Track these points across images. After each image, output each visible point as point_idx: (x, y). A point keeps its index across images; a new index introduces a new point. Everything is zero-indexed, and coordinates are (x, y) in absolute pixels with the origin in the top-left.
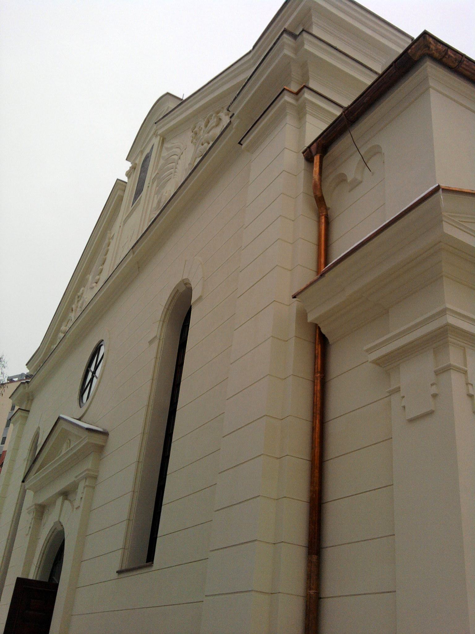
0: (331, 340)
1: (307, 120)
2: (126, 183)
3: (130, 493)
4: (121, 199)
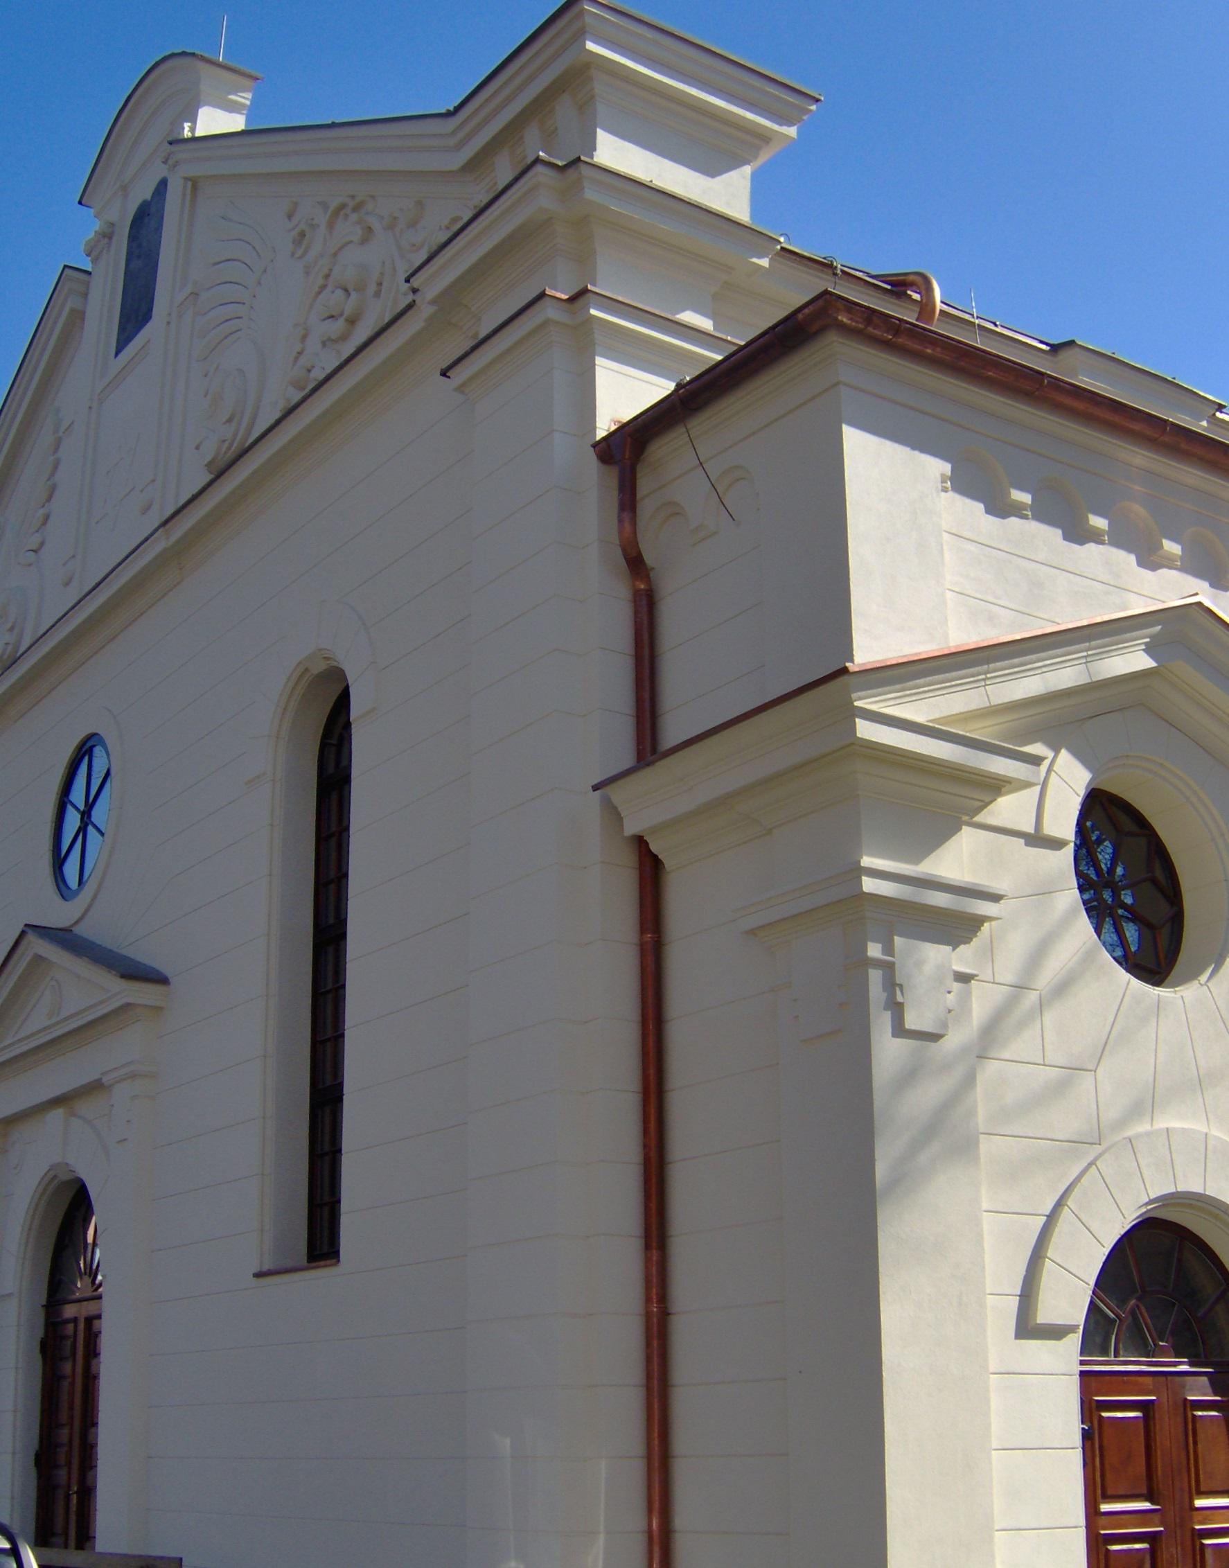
0: (668, 863)
1: (596, 362)
2: (89, 273)
3: (1006, 1054)
4: (78, 317)
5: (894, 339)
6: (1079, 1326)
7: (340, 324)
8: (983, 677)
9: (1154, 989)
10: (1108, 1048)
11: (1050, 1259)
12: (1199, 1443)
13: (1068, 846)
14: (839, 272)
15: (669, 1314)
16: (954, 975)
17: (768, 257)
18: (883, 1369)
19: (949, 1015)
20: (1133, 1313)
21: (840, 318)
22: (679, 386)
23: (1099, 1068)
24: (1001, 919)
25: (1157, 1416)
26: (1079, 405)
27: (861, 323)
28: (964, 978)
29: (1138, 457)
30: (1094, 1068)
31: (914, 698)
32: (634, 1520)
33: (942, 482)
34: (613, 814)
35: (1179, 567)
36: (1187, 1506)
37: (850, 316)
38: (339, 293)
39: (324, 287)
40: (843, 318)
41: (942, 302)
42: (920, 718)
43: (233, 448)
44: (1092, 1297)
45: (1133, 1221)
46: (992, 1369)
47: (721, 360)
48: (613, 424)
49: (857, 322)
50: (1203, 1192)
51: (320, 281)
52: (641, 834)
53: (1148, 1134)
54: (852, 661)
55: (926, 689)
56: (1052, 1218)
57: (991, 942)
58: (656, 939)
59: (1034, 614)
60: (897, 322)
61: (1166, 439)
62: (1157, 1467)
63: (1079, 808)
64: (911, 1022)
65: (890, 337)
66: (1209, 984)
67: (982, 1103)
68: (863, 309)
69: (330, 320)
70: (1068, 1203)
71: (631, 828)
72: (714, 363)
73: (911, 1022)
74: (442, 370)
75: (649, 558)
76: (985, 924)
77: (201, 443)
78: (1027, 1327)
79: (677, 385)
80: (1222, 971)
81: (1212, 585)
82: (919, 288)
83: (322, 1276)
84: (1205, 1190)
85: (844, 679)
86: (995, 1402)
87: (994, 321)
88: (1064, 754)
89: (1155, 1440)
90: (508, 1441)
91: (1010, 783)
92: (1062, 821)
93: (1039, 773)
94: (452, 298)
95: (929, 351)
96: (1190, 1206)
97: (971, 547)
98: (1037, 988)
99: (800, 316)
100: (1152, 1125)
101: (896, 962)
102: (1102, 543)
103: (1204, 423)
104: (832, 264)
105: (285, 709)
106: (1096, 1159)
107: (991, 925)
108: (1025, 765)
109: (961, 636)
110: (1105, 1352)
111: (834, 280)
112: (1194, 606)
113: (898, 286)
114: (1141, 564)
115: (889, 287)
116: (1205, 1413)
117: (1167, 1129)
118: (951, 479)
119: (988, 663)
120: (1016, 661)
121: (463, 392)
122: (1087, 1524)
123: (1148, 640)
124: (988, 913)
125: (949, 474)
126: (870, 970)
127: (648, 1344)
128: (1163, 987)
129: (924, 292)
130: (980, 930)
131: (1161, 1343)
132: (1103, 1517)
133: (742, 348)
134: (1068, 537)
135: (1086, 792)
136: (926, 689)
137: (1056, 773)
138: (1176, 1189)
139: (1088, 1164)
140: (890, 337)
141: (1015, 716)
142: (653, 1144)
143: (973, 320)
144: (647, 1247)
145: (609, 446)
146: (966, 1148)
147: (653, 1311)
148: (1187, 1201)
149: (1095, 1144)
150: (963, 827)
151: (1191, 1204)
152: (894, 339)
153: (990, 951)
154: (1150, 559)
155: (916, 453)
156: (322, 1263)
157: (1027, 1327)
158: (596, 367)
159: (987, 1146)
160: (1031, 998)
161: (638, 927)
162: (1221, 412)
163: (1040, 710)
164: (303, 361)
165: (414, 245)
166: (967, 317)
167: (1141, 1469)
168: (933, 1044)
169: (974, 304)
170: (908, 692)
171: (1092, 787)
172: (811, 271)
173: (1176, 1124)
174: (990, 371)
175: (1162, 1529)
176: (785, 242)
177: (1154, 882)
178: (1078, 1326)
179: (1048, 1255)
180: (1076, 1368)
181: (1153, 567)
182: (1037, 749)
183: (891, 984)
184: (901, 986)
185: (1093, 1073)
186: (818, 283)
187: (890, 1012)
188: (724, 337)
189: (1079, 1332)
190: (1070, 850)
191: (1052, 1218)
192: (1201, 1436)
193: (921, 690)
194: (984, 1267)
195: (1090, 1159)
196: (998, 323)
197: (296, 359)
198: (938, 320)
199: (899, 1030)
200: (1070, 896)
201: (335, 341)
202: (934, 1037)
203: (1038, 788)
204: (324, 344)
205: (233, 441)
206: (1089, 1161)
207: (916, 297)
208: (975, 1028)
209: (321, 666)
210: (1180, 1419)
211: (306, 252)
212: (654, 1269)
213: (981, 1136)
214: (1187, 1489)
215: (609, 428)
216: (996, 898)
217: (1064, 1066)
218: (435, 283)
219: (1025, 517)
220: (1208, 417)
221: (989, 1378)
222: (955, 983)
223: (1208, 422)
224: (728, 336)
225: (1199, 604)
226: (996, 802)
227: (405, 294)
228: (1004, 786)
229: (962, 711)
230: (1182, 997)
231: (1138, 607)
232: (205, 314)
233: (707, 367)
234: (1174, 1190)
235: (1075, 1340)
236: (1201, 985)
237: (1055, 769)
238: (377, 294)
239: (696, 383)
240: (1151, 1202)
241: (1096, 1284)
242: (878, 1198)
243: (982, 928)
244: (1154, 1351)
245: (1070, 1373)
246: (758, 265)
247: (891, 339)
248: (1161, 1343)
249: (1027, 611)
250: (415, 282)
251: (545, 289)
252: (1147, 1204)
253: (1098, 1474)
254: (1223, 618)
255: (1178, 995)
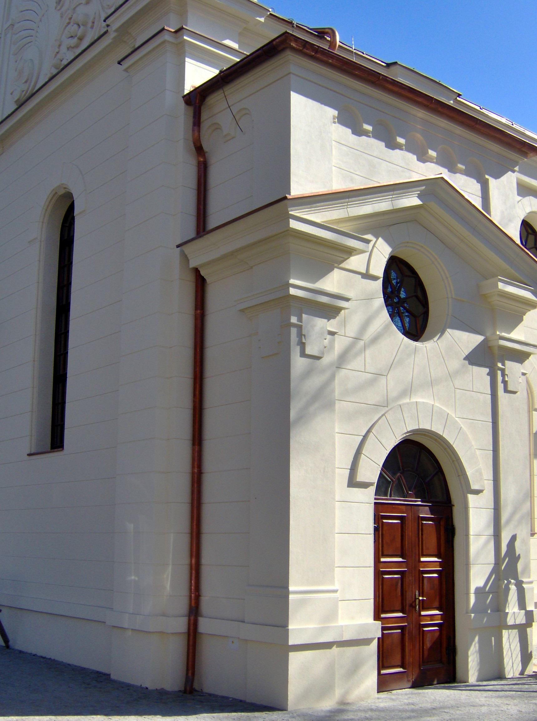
0: (208, 280)
1: (186, 60)
5: (315, 55)
6: (375, 483)
7: (76, 40)
8: (346, 204)
9: (414, 343)
10: (393, 366)
11: (363, 454)
12: (424, 535)
13: (380, 279)
14: (295, 26)
15: (202, 473)
16: (328, 332)
17: (264, 17)
18: (290, 497)
19: (325, 349)
20: (398, 479)
21: (292, 44)
22: (221, 72)
23: (388, 375)
24: (349, 309)
25: (406, 523)
26: (395, 89)
27: (300, 47)
28: (332, 333)
29: (420, 113)
30: (386, 375)
31: (315, 212)
32: (185, 560)
33: (333, 119)
34: (185, 258)
35: (435, 162)
36: (417, 560)
37: (296, 44)
38: (76, 26)
39: (69, 23)
40: (293, 44)
41: (340, 42)
42: (318, 221)
43: (27, 95)
44: (381, 471)
45: (400, 440)
46: (336, 500)
47: (239, 62)
48: (192, 88)
49: (299, 46)
50: (430, 429)
51: (67, 21)
52: (197, 267)
53: (408, 404)
54: (290, 194)
55: (321, 208)
56: (365, 437)
57: (345, 318)
58: (202, 313)
59: (371, 179)
60: (317, 47)
61: (432, 106)
62: (405, 544)
63: (386, 263)
64: (308, 351)
65: (314, 54)
66: (438, 342)
67: (337, 387)
68: (302, 41)
69: (71, 38)
70: (372, 431)
71: (193, 264)
72: (236, 62)
73: (308, 351)
74: (118, 61)
75: (205, 147)
76: (342, 311)
77: (13, 92)
78: (353, 483)
79: (220, 71)
80: (443, 336)
81: (449, 171)
82: (330, 34)
83: (56, 456)
84: (431, 429)
85: (286, 201)
86: (337, 512)
87: (363, 52)
88: (380, 239)
89: (405, 533)
90: (132, 525)
91: (356, 250)
92: (379, 269)
93: (368, 247)
94: (124, 30)
95: (330, 61)
96: (425, 435)
97: (345, 148)
98: (363, 339)
99: (274, 43)
100: (410, 400)
101: (303, 325)
102: (402, 150)
103: (452, 102)
104: (292, 22)
105: (46, 210)
106: (385, 413)
107: (345, 311)
108: (363, 243)
109: (338, 186)
110: (386, 495)
111: (293, 29)
112: (440, 179)
113: (321, 34)
114: (418, 159)
115: (317, 34)
116: (427, 522)
117: (416, 402)
118: (338, 118)
119: (349, 198)
120: (361, 198)
121: (127, 72)
122: (374, 566)
123: (419, 192)
124: (344, 306)
125: (337, 116)
126: (291, 328)
127: (193, 485)
128: (419, 342)
129: (332, 37)
130: (340, 313)
131: (410, 492)
132: (381, 564)
133: (248, 56)
134: (387, 146)
135: (389, 256)
136: (321, 208)
137: (376, 248)
138: (419, 427)
139: (382, 415)
140: (314, 54)
141: (362, 222)
142: (197, 400)
143: (352, 50)
144: (194, 444)
145: (190, 98)
146: (330, 405)
147: (195, 471)
148: (424, 433)
149: (385, 407)
150: (335, 269)
151: (425, 434)
152: (315, 55)
153: (344, 323)
154: (423, 158)
155: (323, 106)
156: (56, 450)
157: (353, 483)
158: (186, 62)
159: (338, 405)
160: (361, 343)
161: (194, 308)
162: (459, 98)
163: (369, 220)
164: (59, 56)
165: (109, 6)
166: (350, 49)
167: (398, 544)
168: (317, 361)
169: (353, 43)
170: (313, 209)
171: (392, 255)
172: (284, 25)
173: (420, 400)
174: (357, 71)
175: (406, 569)
176: (272, 11)
177: (417, 297)
178: (374, 483)
179: (363, 453)
180: (372, 500)
181: (424, 161)
182: (368, 237)
183: (300, 335)
184: (304, 335)
185: (386, 376)
186: (281, 29)
187: (299, 346)
188: (243, 52)
189: (375, 486)
190: (380, 281)
191: (365, 437)
192: (425, 532)
193: (319, 208)
194: (335, 457)
195: (383, 413)
196: (364, 53)
197: (56, 56)
198: (337, 49)
199: (303, 354)
200: (380, 301)
201: (73, 48)
202: (318, 358)
203: (368, 254)
204: (68, 49)
205: (27, 92)
206: (382, 414)
207: (329, 39)
208: (336, 355)
209: (62, 192)
210: (416, 525)
211: (62, 6)
212: (196, 454)
213: (336, 401)
214: (417, 553)
215: (190, 90)
216: (347, 300)
217: (373, 373)
218: (117, 22)
219: (369, 137)
220: (454, 99)
221: (335, 503)
222: (328, 335)
223: (453, 101)
224: (244, 51)
225: (442, 178)
226: (350, 259)
227: (104, 27)
228: (353, 252)
229: (337, 218)
230: (426, 347)
231: (416, 177)
232: (17, 34)
233: (233, 64)
234: (418, 428)
235: (373, 489)
236: (434, 342)
237: (376, 246)
238: (92, 27)
239: (229, 70)
240: (408, 432)
241: (383, 466)
242: (291, 426)
243: (341, 312)
244: (406, 496)
245: (371, 503)
246: (259, 21)
247: (314, 55)
248: (410, 492)
249: (367, 177)
250: (108, 22)
251: (164, 27)
252: (406, 433)
253: (380, 546)
254: (456, 188)
255: (424, 345)
